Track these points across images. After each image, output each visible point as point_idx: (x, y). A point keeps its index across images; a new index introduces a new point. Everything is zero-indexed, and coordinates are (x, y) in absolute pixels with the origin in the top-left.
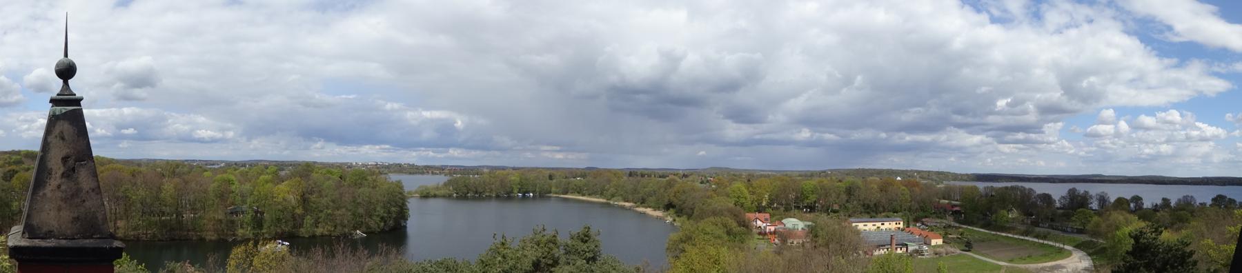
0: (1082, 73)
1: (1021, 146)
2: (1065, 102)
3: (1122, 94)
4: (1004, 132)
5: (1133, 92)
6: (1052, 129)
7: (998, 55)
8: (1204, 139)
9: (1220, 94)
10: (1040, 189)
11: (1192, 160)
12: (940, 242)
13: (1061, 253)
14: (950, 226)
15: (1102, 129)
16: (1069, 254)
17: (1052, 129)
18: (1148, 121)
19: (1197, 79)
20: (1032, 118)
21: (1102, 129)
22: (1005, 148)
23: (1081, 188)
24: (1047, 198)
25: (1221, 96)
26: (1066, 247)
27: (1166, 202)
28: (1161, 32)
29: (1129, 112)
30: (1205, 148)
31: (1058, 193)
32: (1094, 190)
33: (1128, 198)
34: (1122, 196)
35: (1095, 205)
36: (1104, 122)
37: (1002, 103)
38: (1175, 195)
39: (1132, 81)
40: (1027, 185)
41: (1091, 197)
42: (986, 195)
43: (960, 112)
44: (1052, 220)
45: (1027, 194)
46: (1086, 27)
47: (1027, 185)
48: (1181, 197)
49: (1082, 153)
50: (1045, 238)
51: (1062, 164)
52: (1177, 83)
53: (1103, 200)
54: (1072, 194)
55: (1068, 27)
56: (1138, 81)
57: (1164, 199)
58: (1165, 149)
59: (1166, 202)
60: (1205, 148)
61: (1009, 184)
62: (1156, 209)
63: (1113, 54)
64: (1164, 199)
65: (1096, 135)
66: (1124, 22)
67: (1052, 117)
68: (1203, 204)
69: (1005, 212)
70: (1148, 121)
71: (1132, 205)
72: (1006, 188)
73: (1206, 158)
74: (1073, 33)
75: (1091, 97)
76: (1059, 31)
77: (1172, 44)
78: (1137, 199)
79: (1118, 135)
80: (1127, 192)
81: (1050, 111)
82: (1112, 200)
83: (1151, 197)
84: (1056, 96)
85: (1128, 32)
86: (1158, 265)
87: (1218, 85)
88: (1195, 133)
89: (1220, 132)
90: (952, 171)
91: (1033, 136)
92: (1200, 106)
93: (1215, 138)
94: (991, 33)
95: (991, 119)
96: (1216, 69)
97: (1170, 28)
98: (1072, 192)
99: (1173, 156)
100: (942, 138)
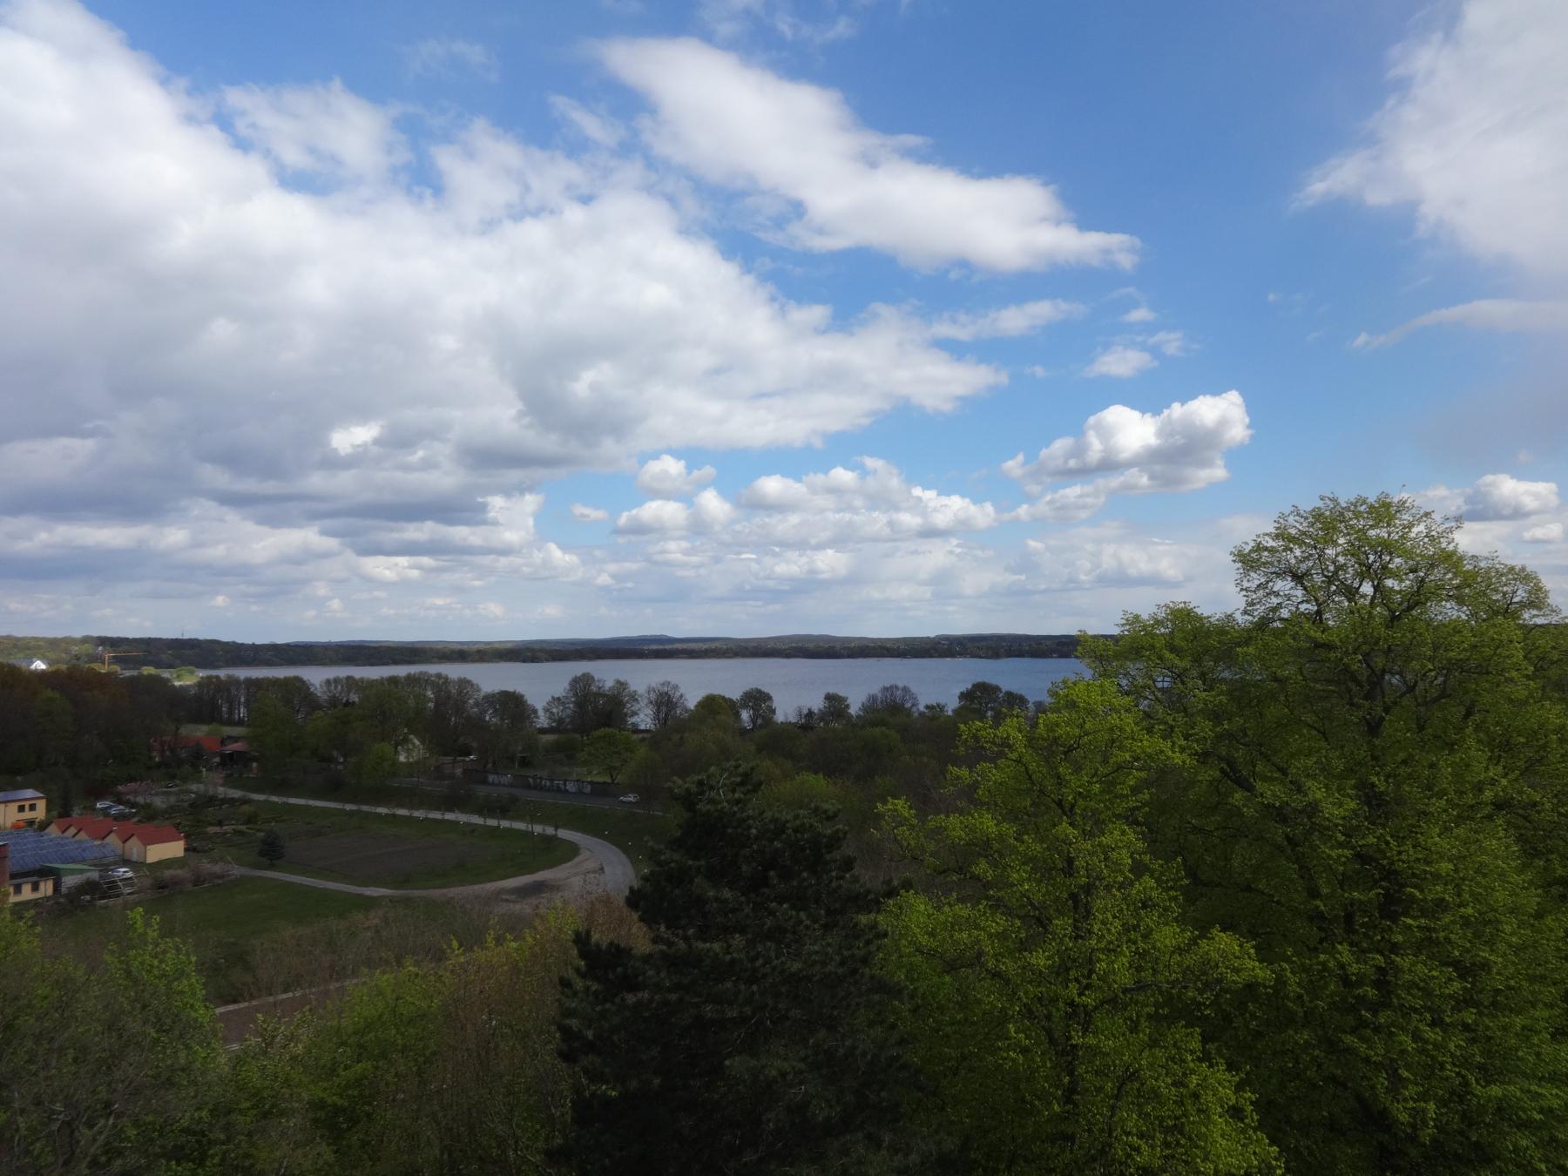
0: (570, 352)
1: (426, 561)
2: (550, 443)
3: (684, 409)
4: (375, 517)
5: (714, 408)
6: (513, 517)
7: (316, 288)
8: (930, 533)
9: (965, 401)
10: (490, 679)
11: (905, 591)
12: (174, 849)
13: (559, 853)
14: (211, 800)
15: (653, 510)
16: (572, 851)
17: (513, 517)
18: (772, 486)
19: (899, 364)
20: (446, 479)
21: (653, 510)
22: (383, 568)
23: (607, 674)
24: (511, 704)
25: (972, 407)
26: (563, 834)
27: (836, 704)
28: (780, 222)
29: (733, 467)
30: (937, 556)
31: (543, 689)
32: (642, 677)
33: (735, 694)
34: (717, 691)
35: (644, 718)
36: (655, 494)
37: (351, 437)
38: (859, 686)
39: (717, 371)
40: (453, 671)
41: (634, 697)
42: (334, 702)
43: (232, 459)
44: (525, 763)
45: (452, 698)
46: (575, 215)
47: (453, 671)
48: (875, 689)
49: (604, 579)
50: (502, 808)
51: (552, 611)
52: (834, 378)
53: (665, 702)
54: (583, 689)
55: (519, 213)
56: (726, 372)
57: (829, 697)
58: (829, 561)
59: (836, 704)
60: (937, 556)
61: (401, 671)
62: (808, 722)
63: (656, 295)
64: (829, 697)
65: (639, 529)
66: (671, 200)
67: (514, 475)
68: (936, 710)
69: (386, 747)
70: (772, 486)
71: (745, 715)
72: (393, 680)
73: (941, 581)
74: (535, 232)
75: (599, 425)
76: (488, 226)
77: (811, 259)
78: (757, 699)
79: (698, 527)
80: (730, 680)
81: (494, 460)
82: (692, 702)
83: (795, 693)
84: (501, 416)
85: (688, 230)
86: (1409, 677)
87: (940, 381)
88: (909, 520)
89: (983, 514)
90: (225, 637)
91: (461, 533)
92: (901, 435)
93: (961, 529)
94: (278, 219)
95: (316, 481)
96: (944, 330)
97: (798, 209)
98: (582, 685)
99: (853, 580)
100: (174, 537)
